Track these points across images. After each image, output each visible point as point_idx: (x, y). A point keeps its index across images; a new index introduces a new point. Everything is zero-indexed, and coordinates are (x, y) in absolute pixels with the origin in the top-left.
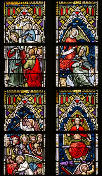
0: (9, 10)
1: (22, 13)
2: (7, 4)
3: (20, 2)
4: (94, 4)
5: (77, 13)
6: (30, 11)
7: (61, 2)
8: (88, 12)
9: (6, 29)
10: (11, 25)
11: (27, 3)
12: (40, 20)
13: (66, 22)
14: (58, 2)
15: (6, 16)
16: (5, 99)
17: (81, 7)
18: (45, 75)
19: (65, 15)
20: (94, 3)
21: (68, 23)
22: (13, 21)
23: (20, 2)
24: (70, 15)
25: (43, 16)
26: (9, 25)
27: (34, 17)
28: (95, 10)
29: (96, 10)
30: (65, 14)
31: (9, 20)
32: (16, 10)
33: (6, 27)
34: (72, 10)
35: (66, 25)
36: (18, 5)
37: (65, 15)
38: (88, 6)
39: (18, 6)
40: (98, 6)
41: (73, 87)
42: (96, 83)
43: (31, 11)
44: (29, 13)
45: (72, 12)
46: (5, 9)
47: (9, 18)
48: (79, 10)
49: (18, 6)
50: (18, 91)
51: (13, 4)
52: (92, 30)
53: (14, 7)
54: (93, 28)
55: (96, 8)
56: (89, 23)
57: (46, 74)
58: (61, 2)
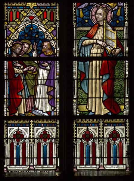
0: (11, 13)
1: (29, 17)
2: (9, 5)
3: (25, 3)
4: (53, 6)
5: (31, 18)
6: (38, 14)
7: (10, 4)
8: (45, 17)
9: (8, 38)
10: (13, 34)
11: (34, 4)
12: (52, 26)
13: (16, 30)
14: (7, 3)
15: (7, 21)
16: (5, 131)
17: (37, 10)
18: (58, 100)
19: (16, 21)
20: (54, 5)
21: (19, 32)
22: (16, 29)
23: (25, 3)
24: (22, 20)
25: (57, 21)
26: (11, 33)
27: (44, 23)
28: (55, 13)
29: (56, 14)
30: (16, 19)
31: (11, 26)
32: (20, 13)
33: (7, 36)
34: (25, 14)
35: (17, 34)
36: (24, 7)
37: (16, 21)
38: (46, 9)
39: (23, 9)
40: (128, 8)
41: (110, 115)
42: (56, 111)
43: (41, 15)
44: (38, 17)
45: (24, 17)
46: (7, 11)
47: (11, 23)
48: (34, 15)
49: (23, 8)
50: (95, 120)
51: (17, 5)
52: (51, 40)
53: (18, 9)
54: (53, 38)
55: (57, 11)
56: (47, 31)
57: (73, 98)
58: (39, 4)
